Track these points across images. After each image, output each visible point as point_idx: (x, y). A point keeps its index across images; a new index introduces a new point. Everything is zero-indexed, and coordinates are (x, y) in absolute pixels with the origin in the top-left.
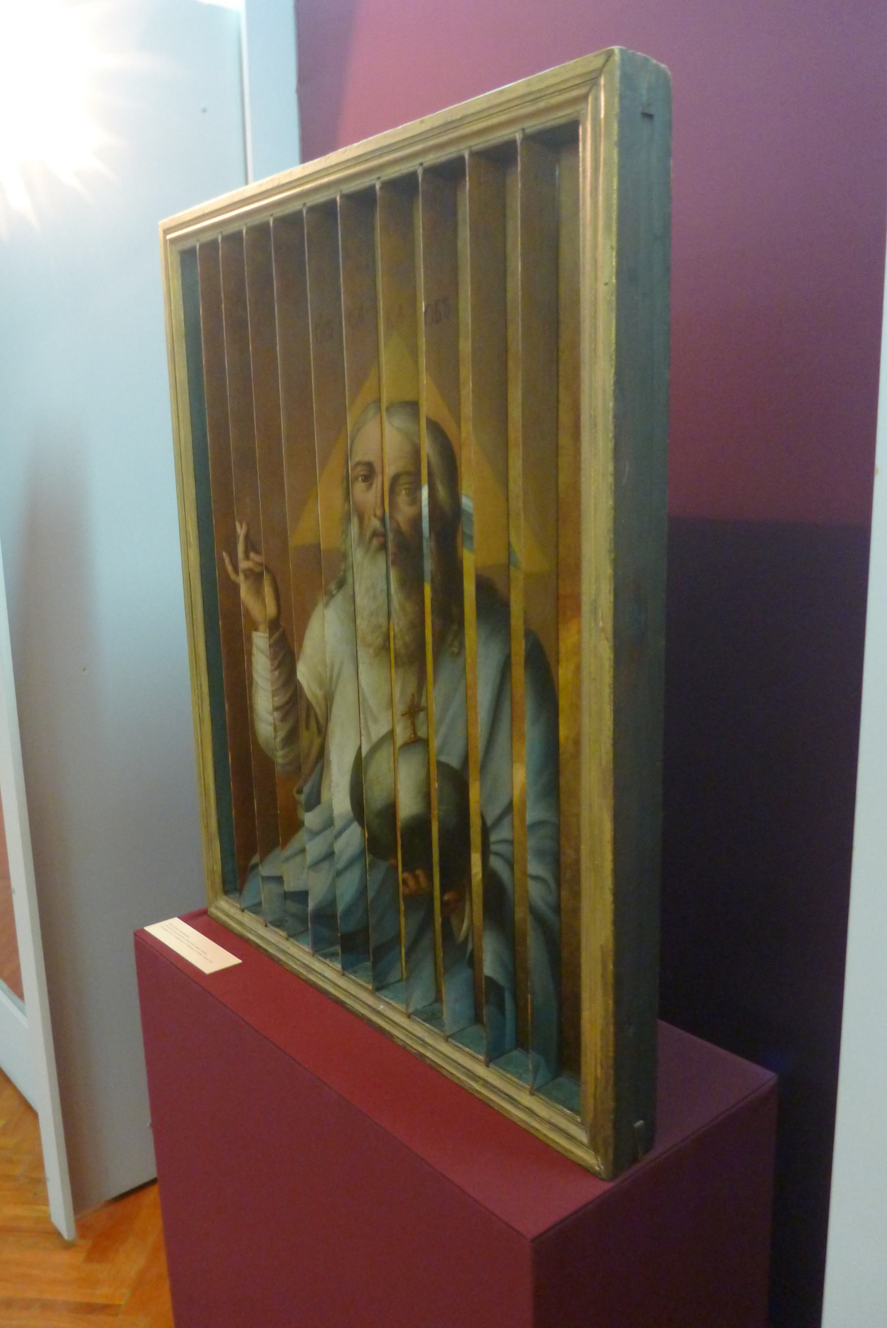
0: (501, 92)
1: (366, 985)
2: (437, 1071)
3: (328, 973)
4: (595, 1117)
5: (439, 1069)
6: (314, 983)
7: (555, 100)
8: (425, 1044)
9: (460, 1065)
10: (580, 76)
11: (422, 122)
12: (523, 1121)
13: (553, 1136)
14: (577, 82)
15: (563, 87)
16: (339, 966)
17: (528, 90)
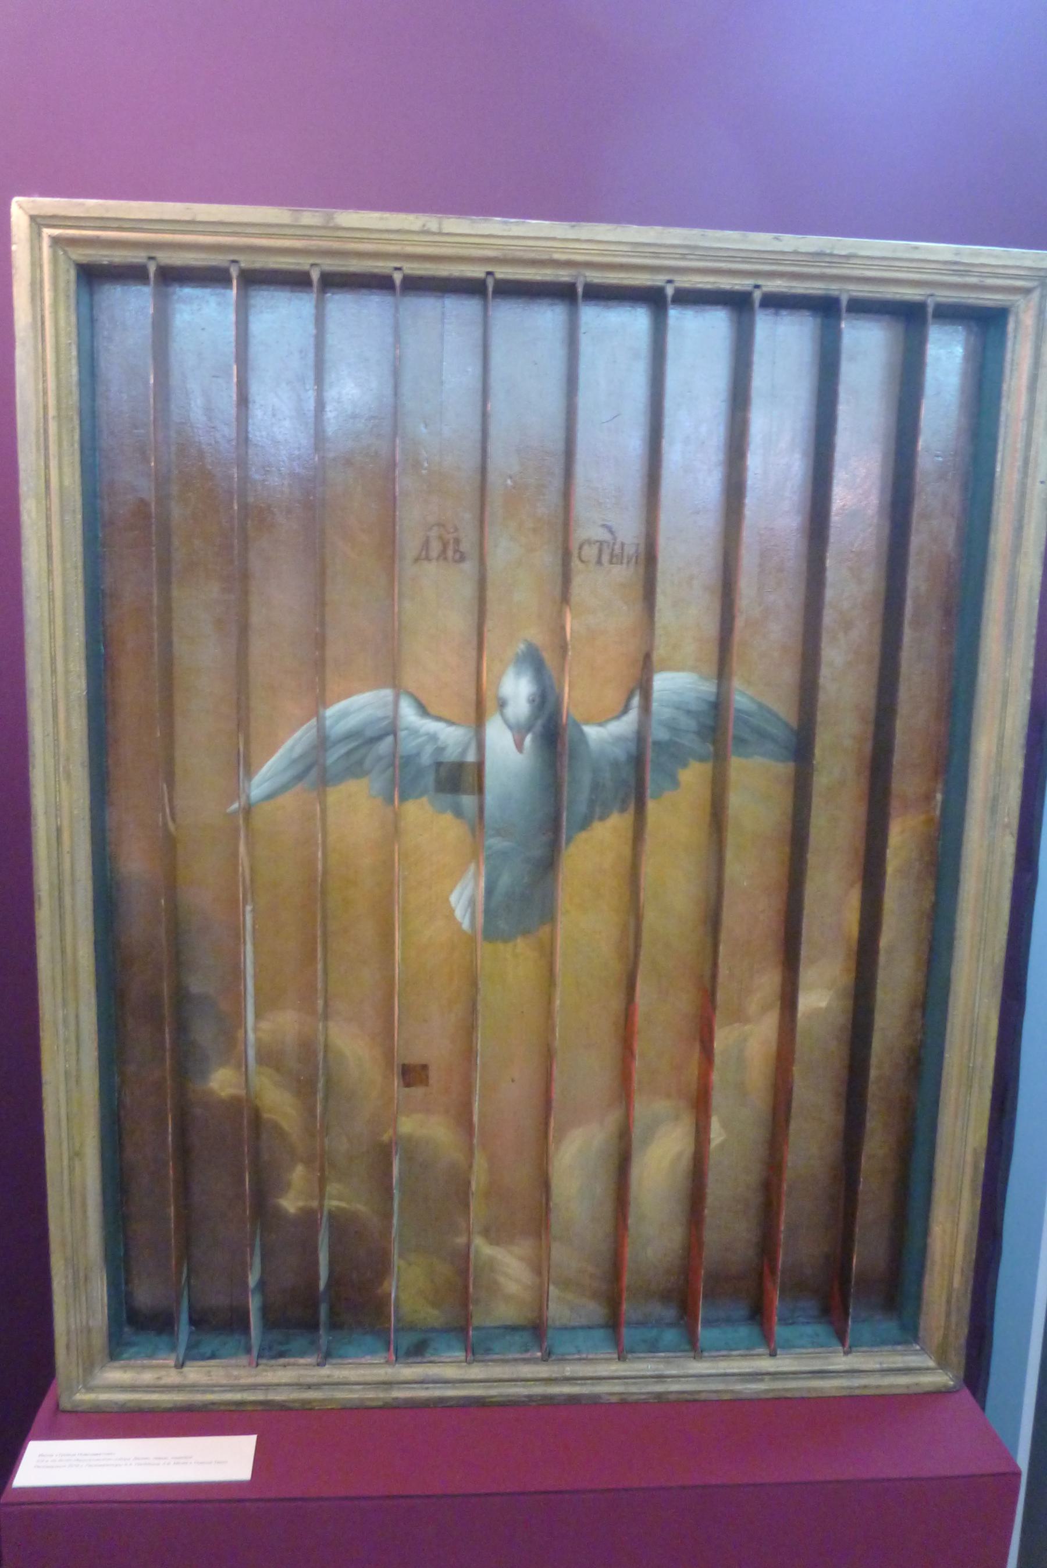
0: (916, 248)
1: (608, 1356)
2: (695, 1401)
3: (450, 1372)
4: (945, 1336)
5: (697, 1397)
6: (407, 1400)
7: (990, 281)
8: (660, 1378)
9: (626, 1378)
10: (1030, 269)
11: (381, 219)
12: (837, 1388)
13: (155, 1397)
14: (1022, 273)
15: (1001, 271)
16: (460, 1355)
17: (957, 259)
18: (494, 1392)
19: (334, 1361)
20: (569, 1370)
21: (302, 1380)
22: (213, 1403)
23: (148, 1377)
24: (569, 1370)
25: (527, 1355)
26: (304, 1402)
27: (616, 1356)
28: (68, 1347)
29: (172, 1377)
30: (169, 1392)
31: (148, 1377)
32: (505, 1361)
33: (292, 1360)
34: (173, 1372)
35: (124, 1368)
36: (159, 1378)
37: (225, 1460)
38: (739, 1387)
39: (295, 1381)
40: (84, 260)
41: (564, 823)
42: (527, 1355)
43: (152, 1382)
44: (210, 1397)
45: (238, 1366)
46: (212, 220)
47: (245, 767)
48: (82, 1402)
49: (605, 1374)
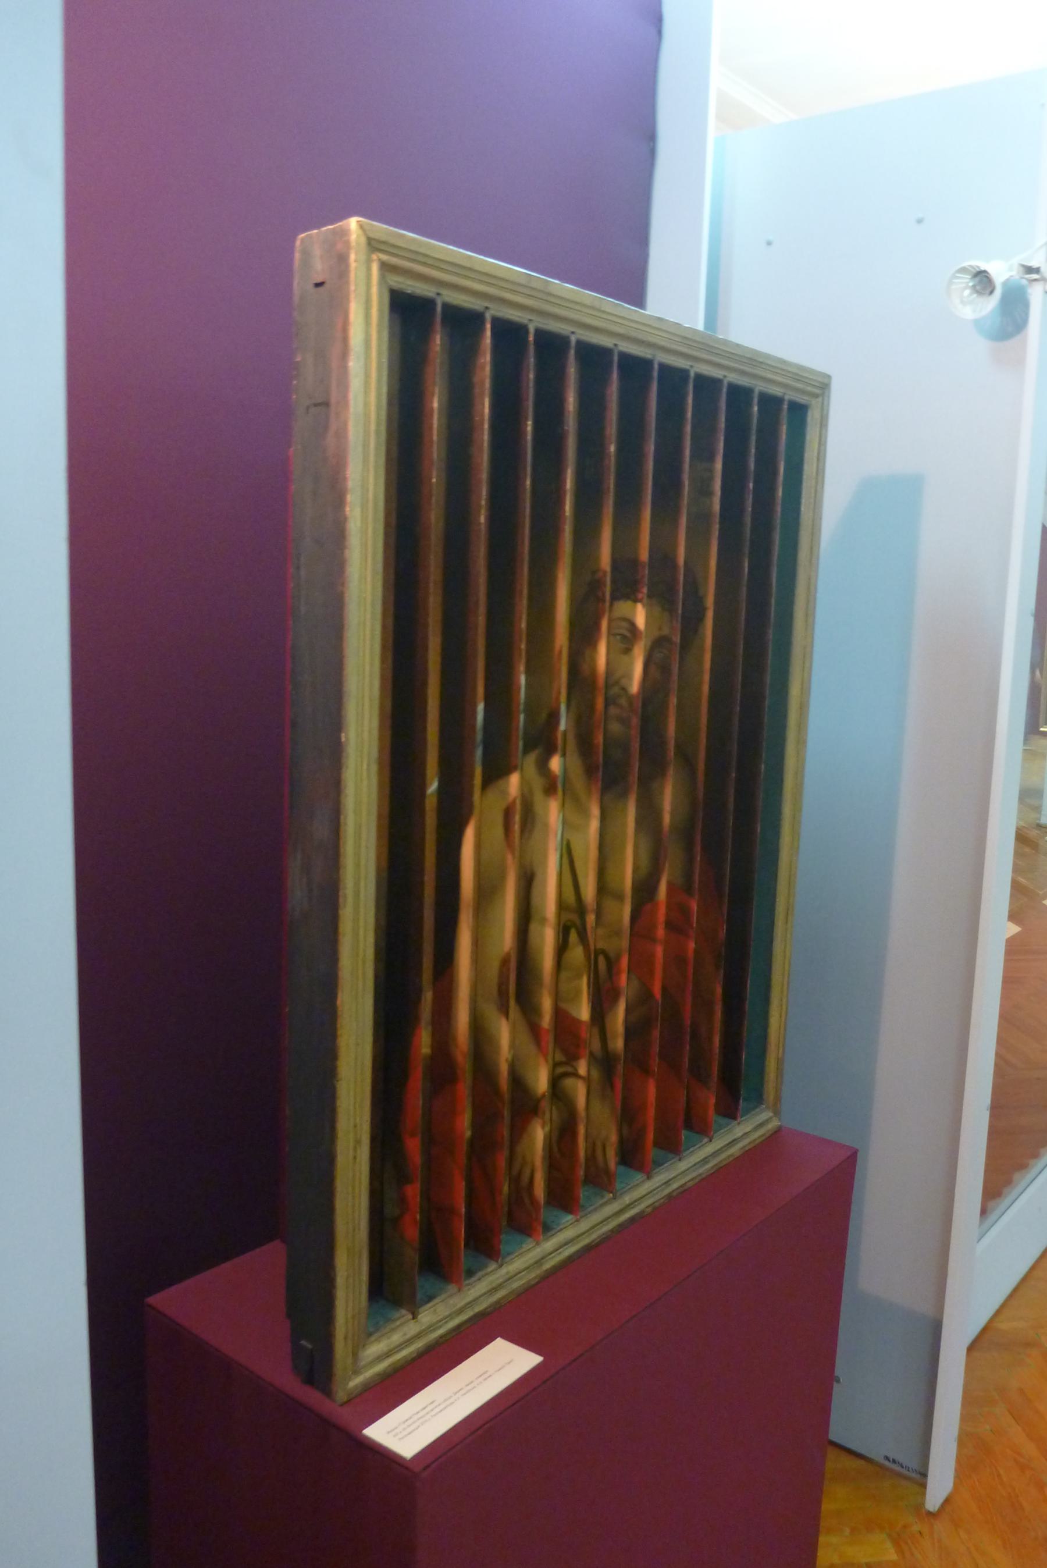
2: (685, 1191)
3: (636, 1194)
18: (594, 1236)
19: (507, 1259)
20: (627, 1199)
21: (494, 1285)
22: (441, 1337)
23: (396, 1338)
24: (627, 1199)
25: (605, 1200)
26: (498, 1302)
27: (411, 1317)
28: (346, 1338)
29: (412, 1328)
30: (412, 1343)
31: (396, 1338)
32: (595, 1210)
33: (480, 1274)
34: (412, 1324)
35: (378, 1340)
36: (405, 1334)
37: (500, 1367)
38: (701, 1171)
39: (490, 1287)
40: (396, 286)
41: (778, 521)
42: (605, 1200)
43: (402, 1340)
44: (441, 1332)
45: (451, 1296)
46: (448, 259)
47: (619, 505)
48: (356, 1386)
49: (644, 1193)
